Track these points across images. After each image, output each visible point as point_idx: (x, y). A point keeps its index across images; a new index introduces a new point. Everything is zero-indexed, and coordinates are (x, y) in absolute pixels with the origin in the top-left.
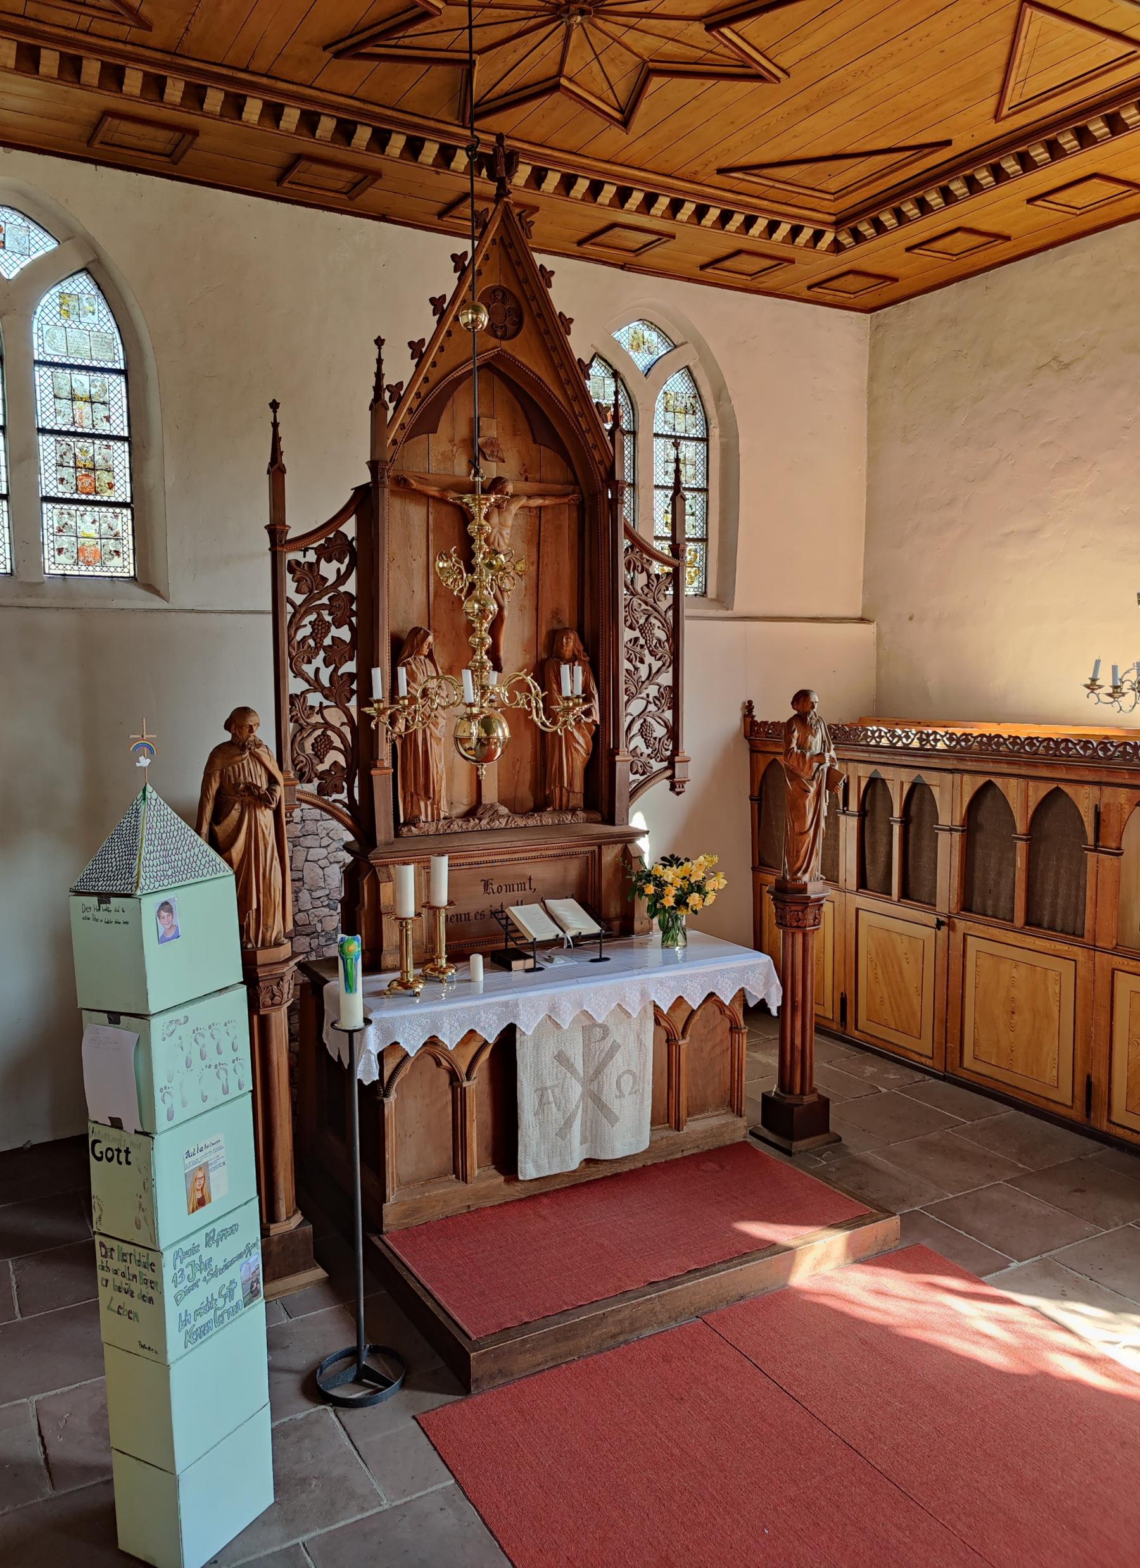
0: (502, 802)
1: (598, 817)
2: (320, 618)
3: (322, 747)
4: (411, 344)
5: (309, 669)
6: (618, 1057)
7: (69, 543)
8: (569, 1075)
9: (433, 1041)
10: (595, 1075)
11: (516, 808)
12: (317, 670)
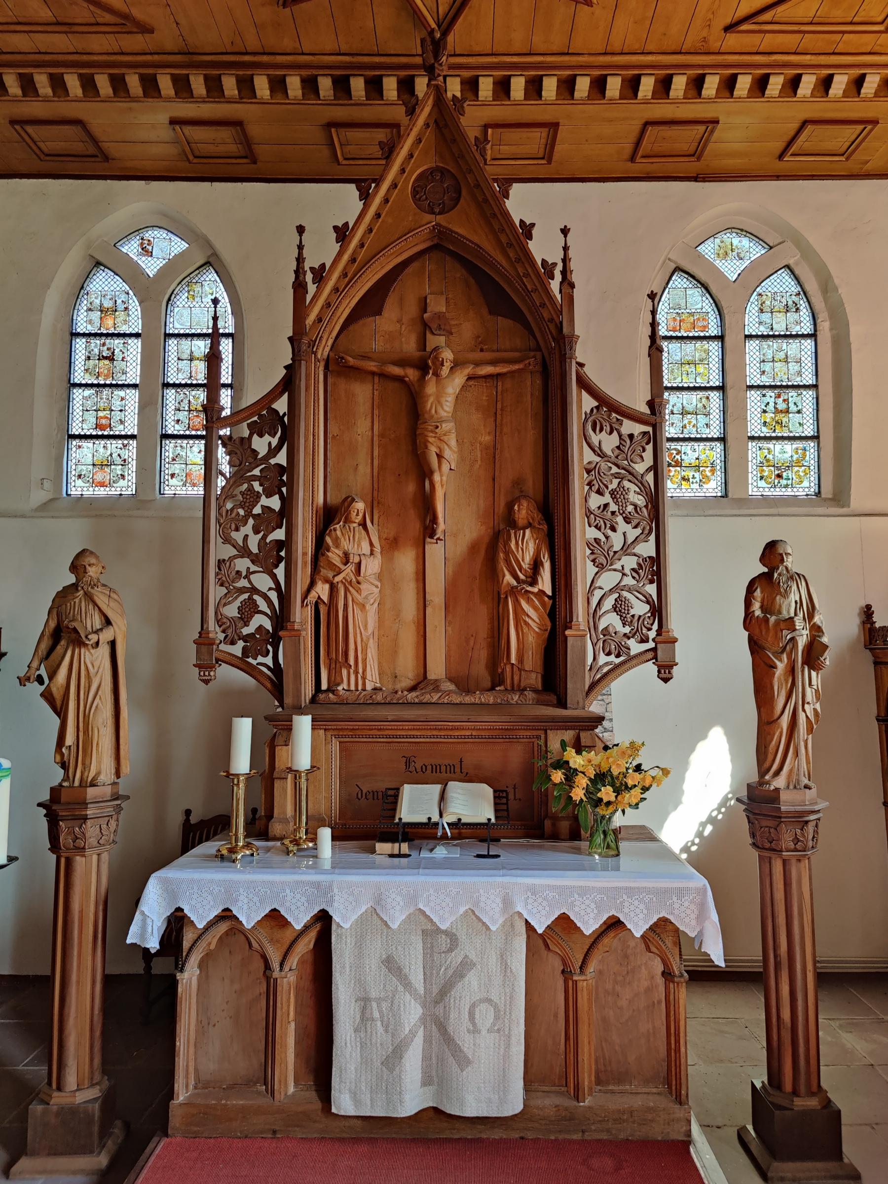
0: (451, 680)
1: (553, 698)
2: (251, 489)
3: (249, 610)
4: (336, 228)
5: (238, 537)
6: (472, 979)
7: (180, 469)
8: (401, 988)
9: (226, 915)
10: (439, 997)
11: (464, 684)
12: (246, 537)
